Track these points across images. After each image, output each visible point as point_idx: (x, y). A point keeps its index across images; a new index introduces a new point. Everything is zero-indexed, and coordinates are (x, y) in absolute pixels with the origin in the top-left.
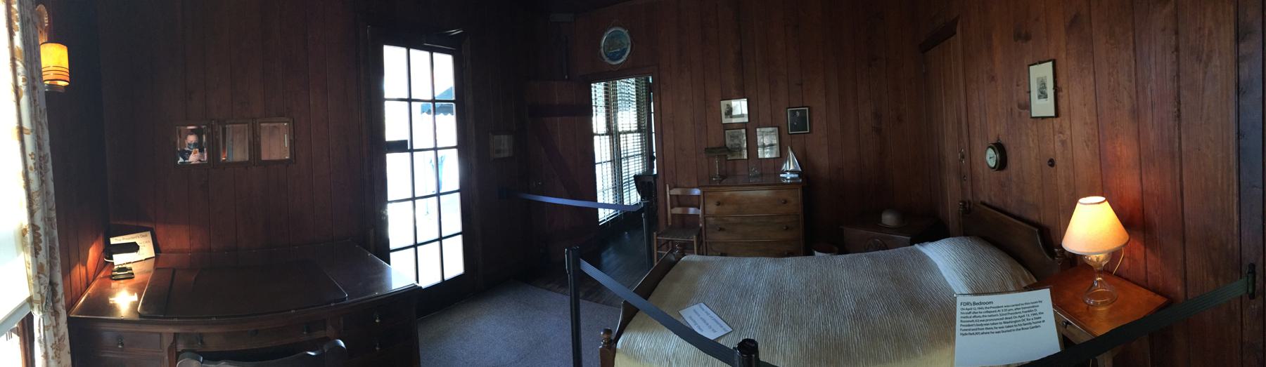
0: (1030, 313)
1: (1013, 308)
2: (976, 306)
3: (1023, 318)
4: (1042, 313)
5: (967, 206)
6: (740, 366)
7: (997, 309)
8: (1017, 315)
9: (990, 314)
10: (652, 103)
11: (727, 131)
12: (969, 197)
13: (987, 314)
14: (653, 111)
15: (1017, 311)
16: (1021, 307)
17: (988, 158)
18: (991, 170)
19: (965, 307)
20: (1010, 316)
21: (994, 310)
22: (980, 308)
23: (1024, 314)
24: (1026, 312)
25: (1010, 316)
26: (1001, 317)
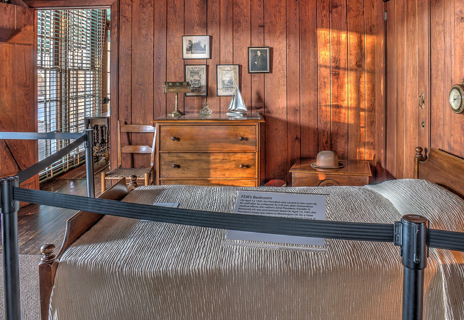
0: (303, 211)
1: (289, 205)
2: (255, 199)
3: (297, 213)
4: (315, 213)
5: (423, 153)
6: (96, 319)
7: (274, 204)
8: (292, 210)
9: (266, 206)
10: (109, 43)
11: (187, 67)
12: (426, 145)
13: (264, 206)
14: (109, 49)
15: (292, 207)
16: (296, 205)
17: (452, 100)
18: (453, 112)
19: (245, 199)
20: (284, 210)
21: (272, 203)
22: (259, 201)
23: (298, 210)
24: (300, 209)
25: (284, 210)
26: (277, 209)
